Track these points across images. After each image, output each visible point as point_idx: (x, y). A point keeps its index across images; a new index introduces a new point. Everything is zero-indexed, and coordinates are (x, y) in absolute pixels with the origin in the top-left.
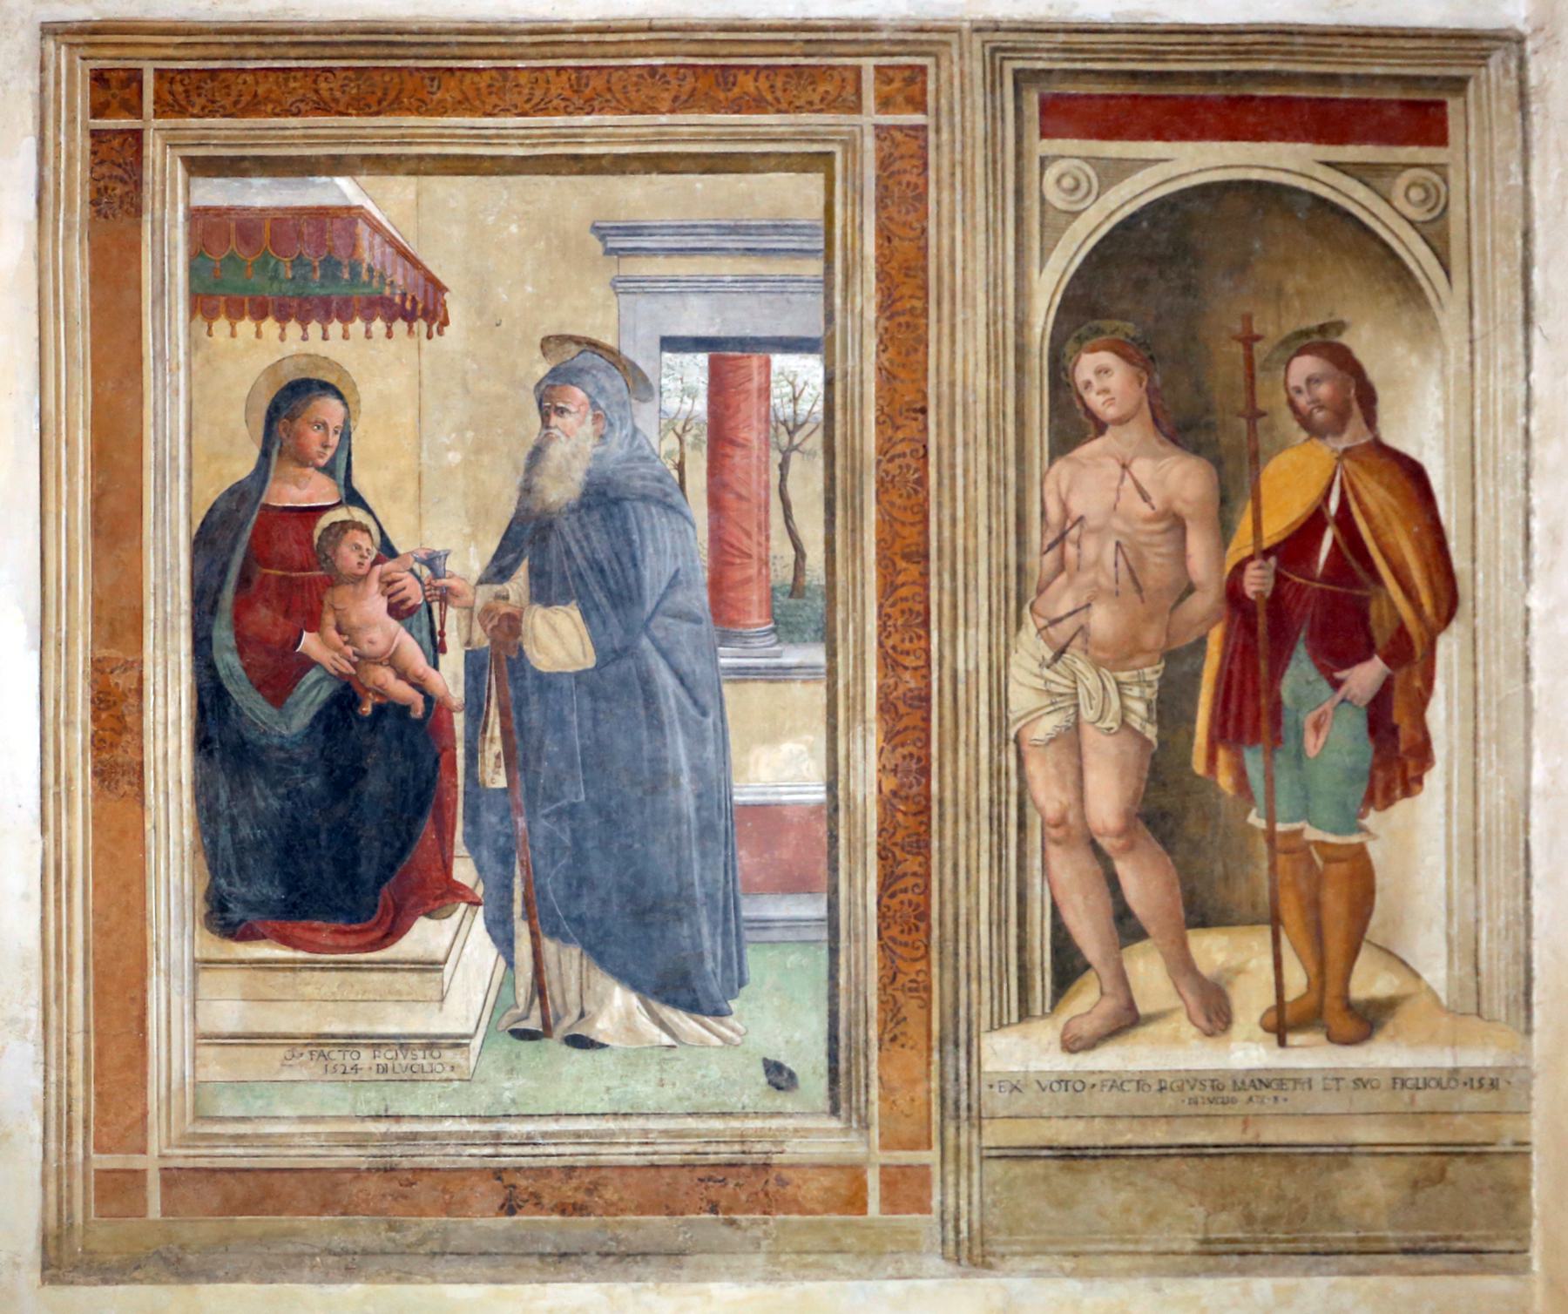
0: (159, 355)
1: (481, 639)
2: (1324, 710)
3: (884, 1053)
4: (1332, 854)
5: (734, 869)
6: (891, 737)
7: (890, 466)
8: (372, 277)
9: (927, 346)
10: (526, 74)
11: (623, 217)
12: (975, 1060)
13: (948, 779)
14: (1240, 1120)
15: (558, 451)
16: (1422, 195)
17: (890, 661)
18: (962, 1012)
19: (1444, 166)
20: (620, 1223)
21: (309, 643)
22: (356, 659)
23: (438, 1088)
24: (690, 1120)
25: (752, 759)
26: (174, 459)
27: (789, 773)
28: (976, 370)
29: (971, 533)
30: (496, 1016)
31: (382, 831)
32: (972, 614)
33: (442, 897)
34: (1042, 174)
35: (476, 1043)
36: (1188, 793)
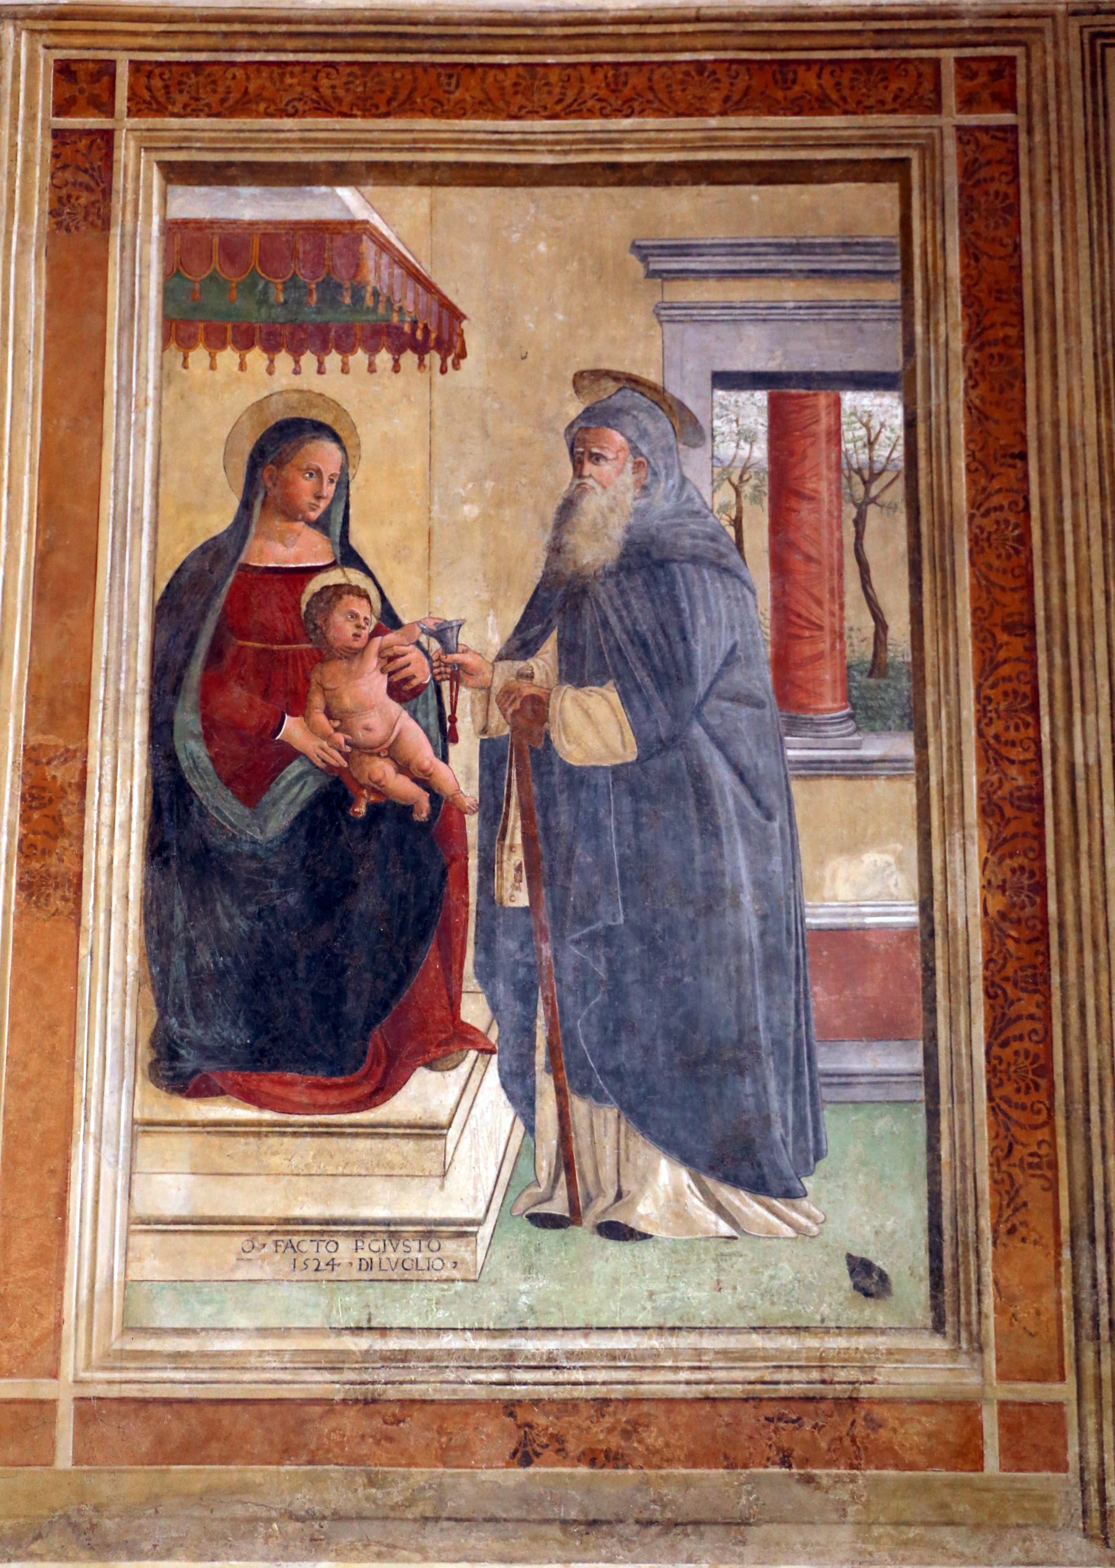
0: (125, 390)
1: (500, 725)
3: (1001, 1249)
5: (807, 1008)
6: (996, 846)
7: (984, 522)
8: (376, 302)
9: (1024, 381)
10: (557, 70)
11: (668, 234)
13: (1069, 898)
15: (593, 504)
17: (992, 754)
18: (1098, 1196)
20: (666, 1479)
21: (292, 729)
22: (348, 749)
23: (436, 1290)
24: (754, 1336)
25: (828, 873)
26: (137, 510)
27: (871, 890)
28: (1083, 408)
30: (512, 1196)
31: (374, 960)
32: (1089, 696)
33: (447, 1042)
35: (485, 1231)
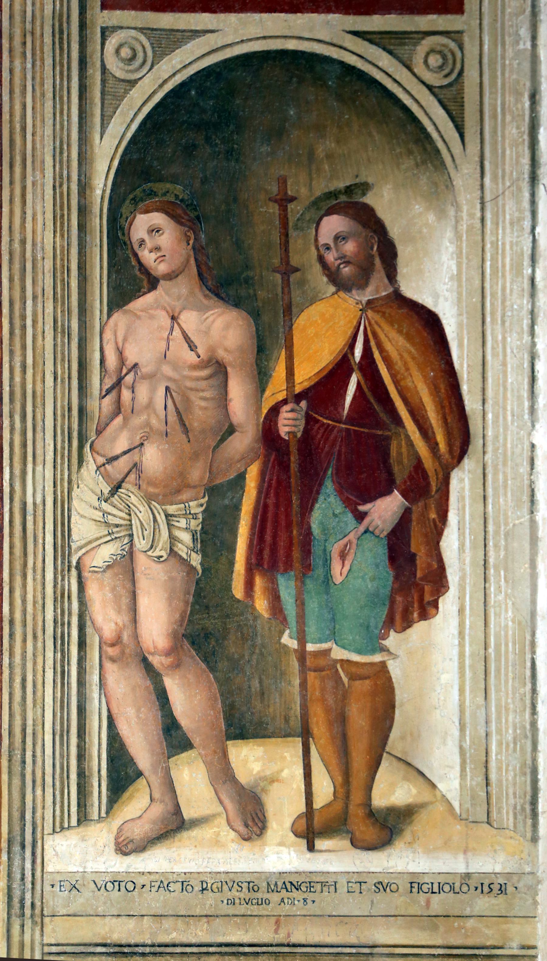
2: (349, 539)
4: (356, 672)
12: (39, 861)
13: (18, 602)
14: (273, 920)
16: (440, 61)
18: (28, 816)
19: (460, 32)
29: (39, 378)
32: (39, 452)
34: (103, 44)
36: (228, 616)
